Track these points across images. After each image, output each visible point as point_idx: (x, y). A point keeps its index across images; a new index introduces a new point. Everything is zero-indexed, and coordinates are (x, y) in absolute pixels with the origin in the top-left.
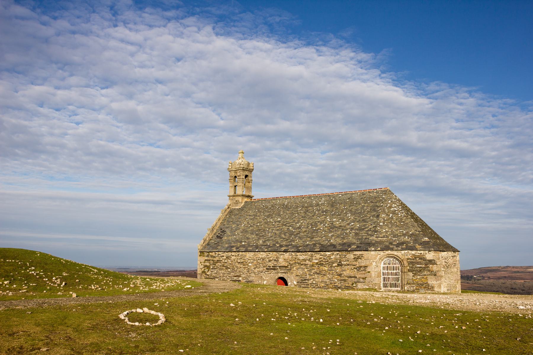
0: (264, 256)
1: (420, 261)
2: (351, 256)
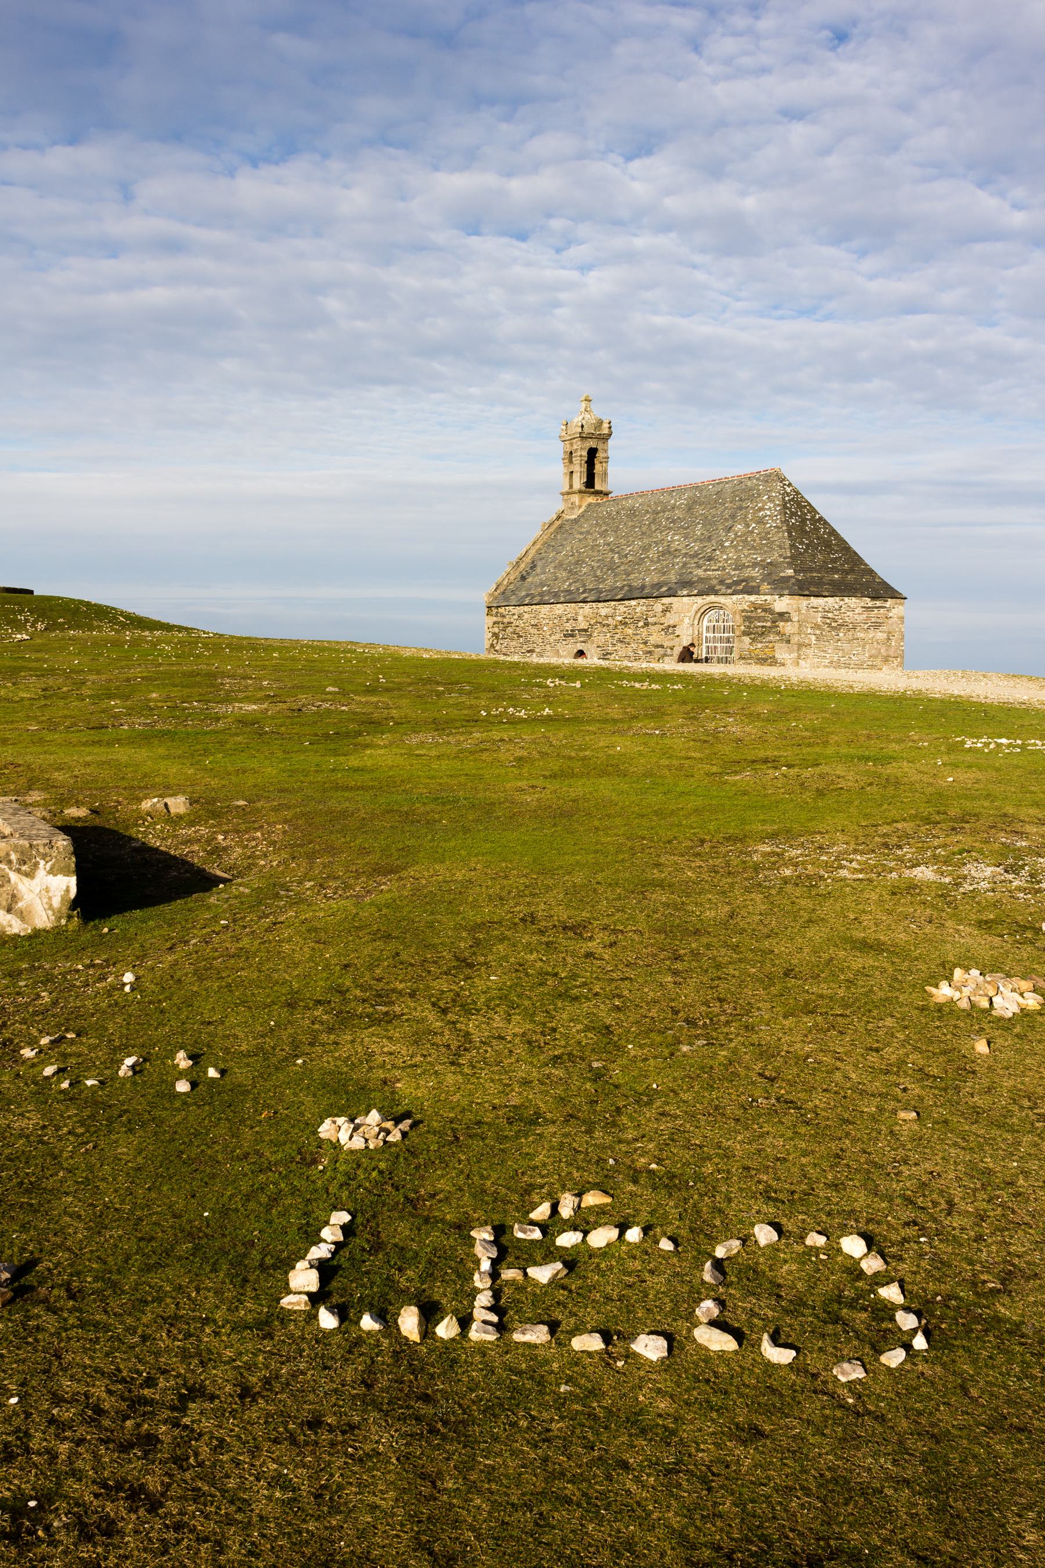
0: (560, 612)
1: (763, 614)
2: (658, 607)
